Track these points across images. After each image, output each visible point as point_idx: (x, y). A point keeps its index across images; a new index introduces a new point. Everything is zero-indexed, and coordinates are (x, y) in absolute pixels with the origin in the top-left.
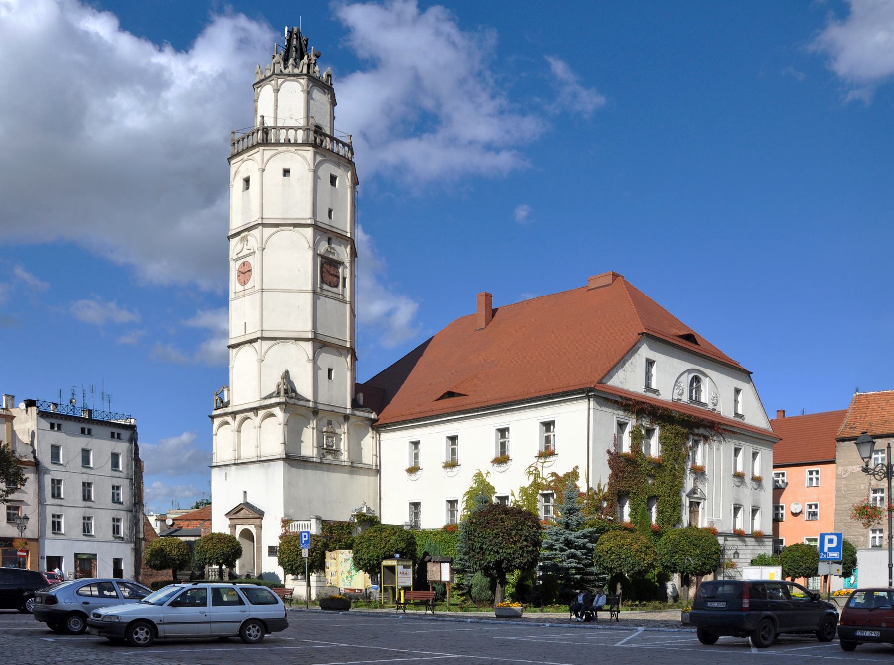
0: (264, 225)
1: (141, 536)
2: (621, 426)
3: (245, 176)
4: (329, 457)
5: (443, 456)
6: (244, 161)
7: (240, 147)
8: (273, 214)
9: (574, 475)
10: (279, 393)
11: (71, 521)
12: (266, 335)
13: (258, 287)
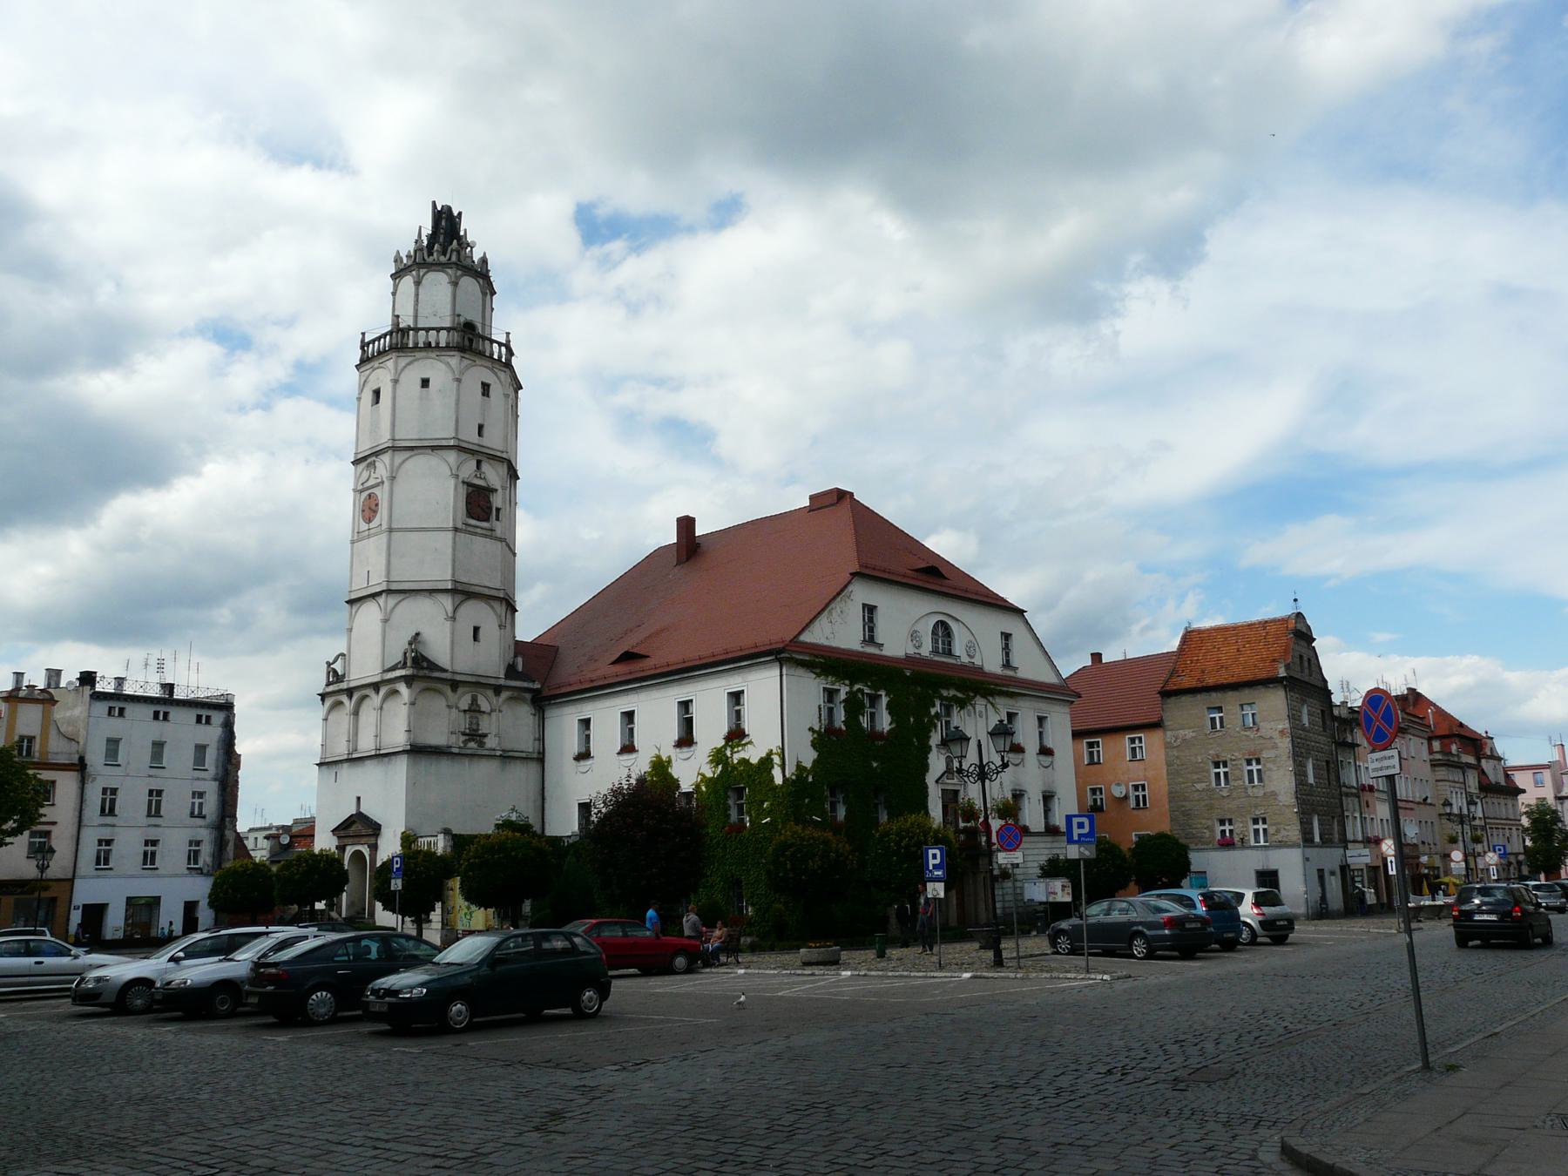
0: (394, 449)
2: (831, 694)
4: (472, 745)
5: (574, 747)
8: (408, 434)
9: (766, 762)
11: (128, 846)
12: (394, 587)
13: (385, 526)
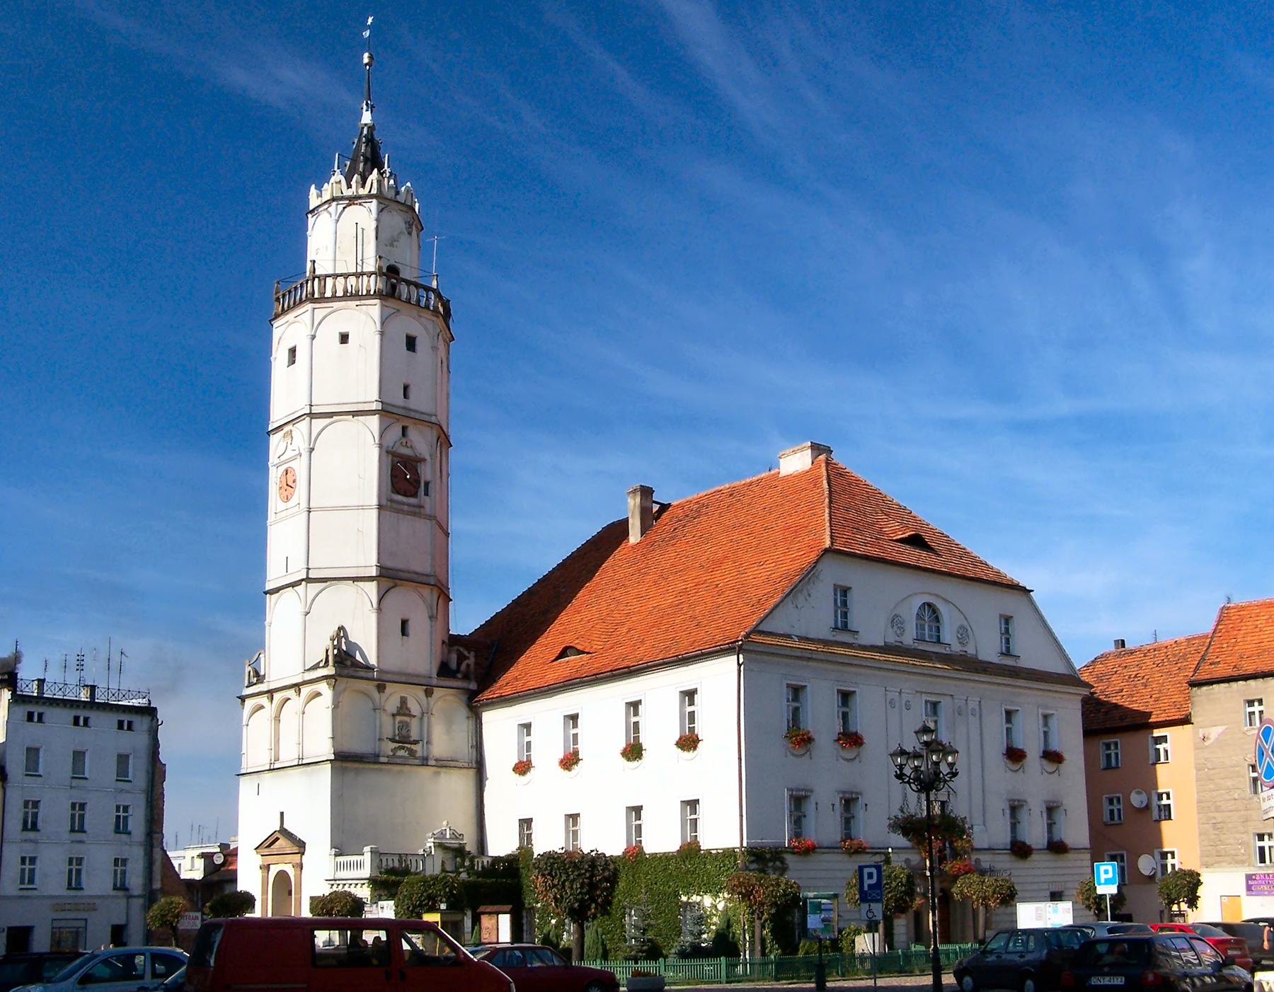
0: (312, 415)
1: (157, 885)
3: (291, 346)
6: (289, 323)
7: (360, 231)
10: (327, 661)
